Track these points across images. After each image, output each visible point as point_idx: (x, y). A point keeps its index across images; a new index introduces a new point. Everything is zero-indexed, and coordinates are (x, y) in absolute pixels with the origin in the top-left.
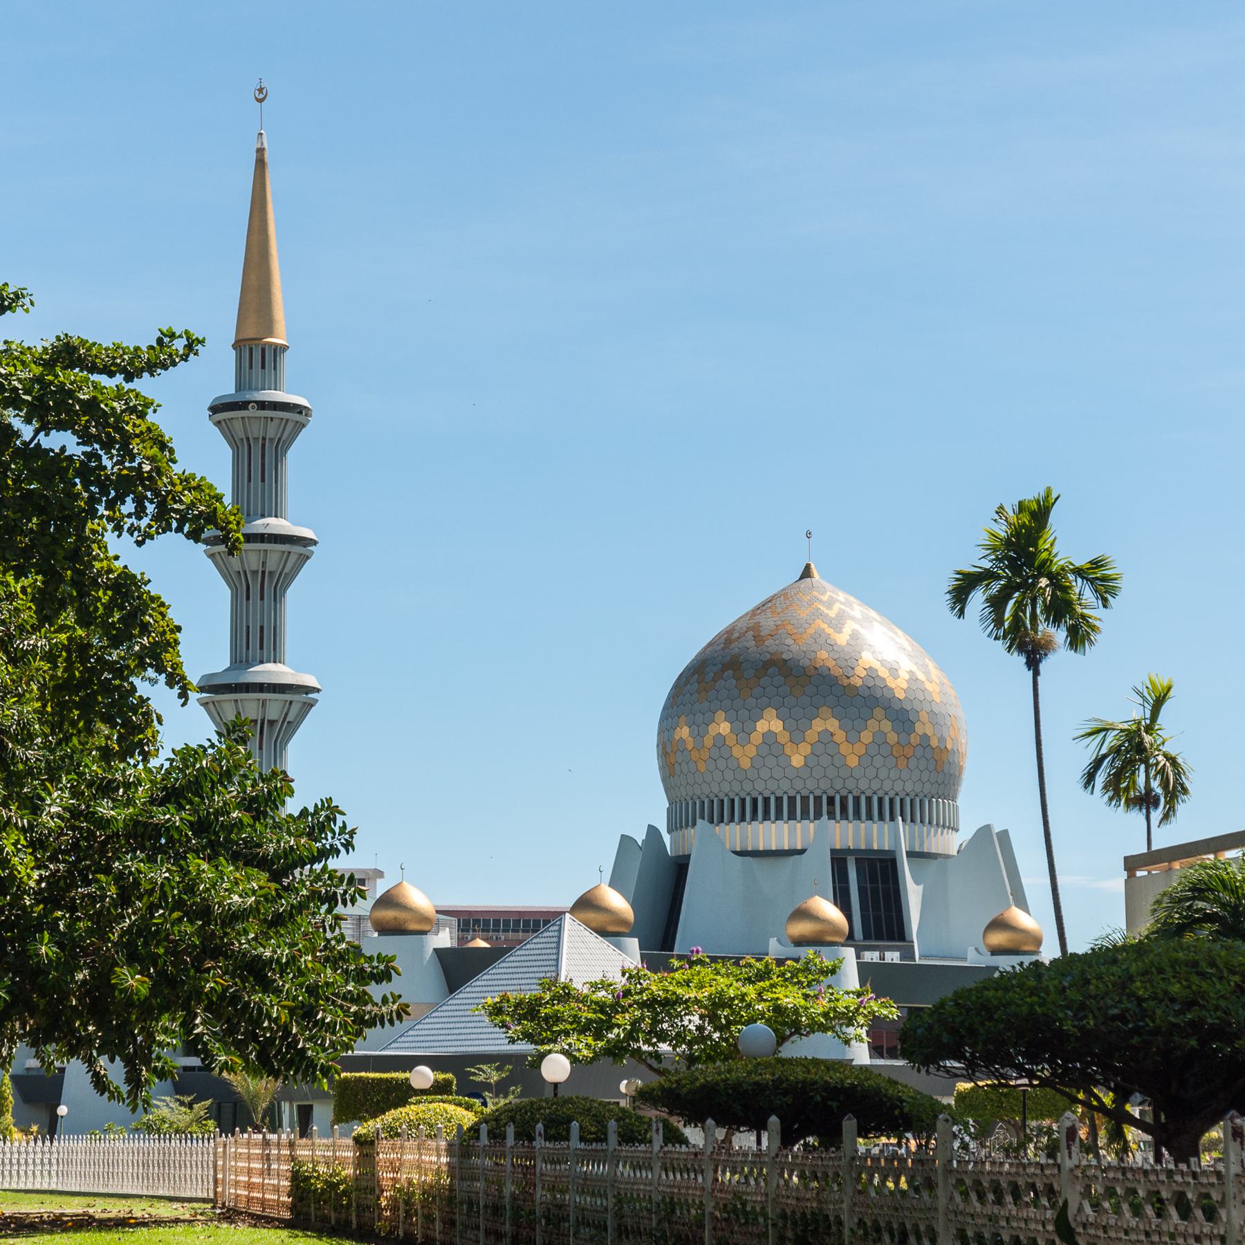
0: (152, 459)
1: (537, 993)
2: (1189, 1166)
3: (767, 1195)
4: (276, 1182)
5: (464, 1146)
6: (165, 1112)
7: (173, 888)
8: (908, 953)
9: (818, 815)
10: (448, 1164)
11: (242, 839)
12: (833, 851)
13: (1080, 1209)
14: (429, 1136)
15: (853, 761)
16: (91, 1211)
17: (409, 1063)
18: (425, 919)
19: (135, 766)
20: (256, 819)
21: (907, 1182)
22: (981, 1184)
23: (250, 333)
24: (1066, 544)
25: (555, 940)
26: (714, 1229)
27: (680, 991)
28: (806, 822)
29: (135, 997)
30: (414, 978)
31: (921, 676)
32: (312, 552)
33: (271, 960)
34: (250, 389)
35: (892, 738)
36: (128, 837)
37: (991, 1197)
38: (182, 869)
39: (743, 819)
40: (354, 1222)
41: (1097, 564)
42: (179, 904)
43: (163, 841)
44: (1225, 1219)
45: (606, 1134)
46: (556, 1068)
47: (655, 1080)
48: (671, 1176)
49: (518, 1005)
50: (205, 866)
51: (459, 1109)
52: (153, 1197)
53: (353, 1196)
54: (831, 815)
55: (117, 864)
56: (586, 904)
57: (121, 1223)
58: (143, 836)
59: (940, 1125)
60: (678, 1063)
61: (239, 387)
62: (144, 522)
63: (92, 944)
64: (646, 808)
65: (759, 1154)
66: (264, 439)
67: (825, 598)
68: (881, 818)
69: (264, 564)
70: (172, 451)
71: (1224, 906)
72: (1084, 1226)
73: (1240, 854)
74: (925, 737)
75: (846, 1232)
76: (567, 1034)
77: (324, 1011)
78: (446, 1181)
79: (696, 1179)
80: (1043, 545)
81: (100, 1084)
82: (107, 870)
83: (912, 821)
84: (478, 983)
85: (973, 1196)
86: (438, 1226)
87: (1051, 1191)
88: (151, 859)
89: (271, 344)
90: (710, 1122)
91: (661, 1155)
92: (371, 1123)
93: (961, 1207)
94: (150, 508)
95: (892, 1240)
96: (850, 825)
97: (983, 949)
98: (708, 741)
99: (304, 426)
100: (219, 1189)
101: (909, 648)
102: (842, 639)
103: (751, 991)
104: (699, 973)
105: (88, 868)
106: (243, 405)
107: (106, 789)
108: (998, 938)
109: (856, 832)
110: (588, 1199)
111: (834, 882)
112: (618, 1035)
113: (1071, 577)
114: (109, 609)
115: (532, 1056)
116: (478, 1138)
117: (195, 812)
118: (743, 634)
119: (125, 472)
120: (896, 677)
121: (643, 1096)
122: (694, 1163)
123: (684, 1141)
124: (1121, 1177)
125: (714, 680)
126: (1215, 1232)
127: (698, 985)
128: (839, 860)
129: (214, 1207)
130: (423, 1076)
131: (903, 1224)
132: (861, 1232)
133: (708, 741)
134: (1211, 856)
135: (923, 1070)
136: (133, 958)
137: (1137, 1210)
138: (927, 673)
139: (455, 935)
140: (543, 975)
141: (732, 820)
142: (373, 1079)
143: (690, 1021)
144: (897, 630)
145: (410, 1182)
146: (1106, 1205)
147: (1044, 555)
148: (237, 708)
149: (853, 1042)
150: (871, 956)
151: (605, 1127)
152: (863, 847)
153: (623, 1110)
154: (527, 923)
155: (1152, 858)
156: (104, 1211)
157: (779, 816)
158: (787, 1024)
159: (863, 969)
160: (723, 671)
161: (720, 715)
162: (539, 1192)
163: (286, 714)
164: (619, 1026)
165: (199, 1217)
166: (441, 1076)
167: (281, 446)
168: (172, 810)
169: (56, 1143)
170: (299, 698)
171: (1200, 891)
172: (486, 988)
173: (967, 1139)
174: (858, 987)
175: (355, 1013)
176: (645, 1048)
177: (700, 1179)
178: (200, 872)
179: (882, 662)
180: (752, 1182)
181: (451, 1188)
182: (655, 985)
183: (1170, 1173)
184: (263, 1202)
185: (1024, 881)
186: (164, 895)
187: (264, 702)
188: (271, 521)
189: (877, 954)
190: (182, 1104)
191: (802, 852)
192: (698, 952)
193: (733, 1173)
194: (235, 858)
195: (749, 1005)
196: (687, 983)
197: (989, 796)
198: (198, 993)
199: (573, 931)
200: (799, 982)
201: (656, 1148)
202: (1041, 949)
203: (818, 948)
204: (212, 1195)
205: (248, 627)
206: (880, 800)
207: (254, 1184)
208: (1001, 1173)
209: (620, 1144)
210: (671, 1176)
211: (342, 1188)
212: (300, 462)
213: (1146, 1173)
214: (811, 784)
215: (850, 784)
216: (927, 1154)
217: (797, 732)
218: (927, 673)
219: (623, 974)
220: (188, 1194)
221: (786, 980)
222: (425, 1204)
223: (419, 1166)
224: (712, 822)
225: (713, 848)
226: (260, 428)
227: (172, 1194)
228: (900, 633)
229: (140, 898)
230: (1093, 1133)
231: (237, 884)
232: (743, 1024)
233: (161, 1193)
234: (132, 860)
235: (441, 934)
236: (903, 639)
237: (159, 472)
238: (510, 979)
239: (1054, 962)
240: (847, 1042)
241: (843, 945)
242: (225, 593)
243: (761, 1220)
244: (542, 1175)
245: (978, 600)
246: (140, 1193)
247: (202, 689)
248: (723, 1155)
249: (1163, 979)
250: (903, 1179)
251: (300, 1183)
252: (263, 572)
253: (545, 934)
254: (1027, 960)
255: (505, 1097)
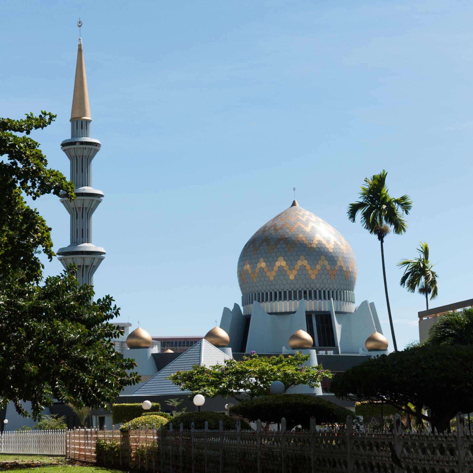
0: (36, 165)
1: (191, 370)
2: (443, 434)
3: (281, 449)
4: (90, 448)
5: (163, 432)
6: (46, 421)
7: (48, 332)
8: (336, 351)
9: (300, 298)
10: (157, 439)
11: (75, 313)
12: (306, 312)
13: (402, 452)
14: (150, 428)
15: (313, 277)
16: (17, 461)
17: (142, 399)
18: (147, 342)
19: (33, 285)
20: (80, 304)
21: (335, 442)
22: (364, 442)
23: (77, 116)
24: (392, 191)
25: (199, 349)
26: (261, 463)
27: (247, 368)
28: (285, 301)
29: (32, 375)
30: (143, 365)
31: (339, 243)
32: (102, 200)
33: (87, 359)
34: (77, 137)
35: (328, 267)
36: (30, 313)
37: (368, 448)
38: (51, 324)
39: (271, 300)
40: (121, 463)
41: (403, 198)
42: (50, 338)
43: (44, 314)
44: (458, 454)
45: (219, 426)
46: (199, 400)
47: (238, 404)
48: (244, 442)
49: (184, 375)
50: (60, 323)
51: (162, 417)
52: (42, 455)
53: (120, 453)
54: (305, 298)
55: (25, 324)
56: (211, 335)
57: (28, 466)
58: (36, 312)
59: (348, 420)
60: (247, 396)
61: (73, 136)
62: (36, 190)
63: (16, 355)
64: (233, 297)
65: (278, 433)
66: (82, 156)
67: (301, 214)
68: (325, 298)
69: (83, 205)
70: (46, 161)
71: (457, 330)
72: (404, 458)
73: (462, 310)
74: (341, 267)
75: (312, 463)
76: (204, 386)
77: (108, 379)
78: (156, 446)
79: (254, 443)
80: (384, 191)
81: (19, 410)
82: (22, 326)
83: (337, 299)
84: (169, 367)
85: (361, 448)
86: (154, 464)
87: (391, 445)
88: (39, 321)
89: (85, 120)
90: (259, 420)
91: (240, 434)
92: (127, 424)
93: (357, 452)
94: (37, 185)
95: (330, 466)
96: (313, 302)
97: (365, 349)
98: (257, 270)
99: (98, 151)
100: (68, 451)
101: (334, 233)
102: (308, 229)
103: (275, 368)
104: (255, 361)
105: (14, 325)
106: (74, 143)
107: (21, 294)
108: (371, 345)
109: (315, 304)
110: (212, 452)
111: (307, 324)
112: (224, 386)
113: (394, 203)
114: (22, 224)
115: (190, 395)
116: (169, 429)
117: (56, 302)
118: (270, 228)
119: (26, 170)
120: (329, 244)
121: (232, 411)
122: (254, 436)
123: (249, 428)
124: (417, 439)
125: (259, 246)
126: (454, 459)
127: (254, 365)
128: (309, 315)
129: (66, 459)
130: (148, 404)
131: (334, 459)
132: (318, 463)
133: (257, 270)
134: (452, 311)
135: (341, 398)
136: (32, 360)
137: (424, 452)
138: (341, 242)
139: (160, 348)
140: (194, 363)
141: (267, 300)
142: (128, 406)
143: (252, 380)
144: (329, 225)
145: (142, 446)
146: (412, 450)
147: (384, 196)
148: (73, 261)
149: (315, 387)
150: (322, 353)
151: (218, 423)
152: (318, 310)
153: (226, 416)
154: (188, 342)
155: (428, 312)
156: (22, 461)
157: (285, 299)
158: (289, 381)
159: (320, 358)
160: (262, 242)
161: (262, 260)
162: (193, 450)
163: (93, 263)
164: (224, 383)
165: (60, 463)
166: (155, 404)
167: (89, 159)
168: (47, 301)
169: (3, 434)
170: (97, 257)
171: (447, 324)
172: (171, 370)
173: (359, 425)
174: (317, 365)
175: (120, 380)
176: (235, 391)
177: (255, 443)
178: (58, 325)
179: (324, 238)
180: (276, 444)
181: (159, 449)
182: (238, 366)
183: (436, 437)
184: (85, 456)
185: (381, 322)
186: (44, 335)
187: (84, 258)
188: (86, 188)
189: (324, 352)
190: (53, 417)
191: (294, 312)
192: (254, 353)
193: (268, 440)
194: (72, 320)
195: (274, 373)
196: (250, 365)
197: (365, 290)
198: (57, 373)
199: (206, 346)
200: (294, 364)
201: (238, 431)
202: (388, 348)
203: (300, 350)
204: (65, 454)
205: (77, 229)
206: (324, 292)
207: (81, 449)
208: (371, 438)
209: (224, 430)
210: (244, 442)
211: (116, 449)
212: (97, 165)
213: (427, 437)
214: (297, 286)
215: (313, 286)
216: (343, 431)
217: (291, 266)
218: (341, 242)
219: (225, 362)
220: (56, 454)
221: (289, 363)
222: (148, 455)
223: (146, 440)
224: (259, 301)
225: (260, 311)
226: (81, 151)
227: (49, 453)
228: (331, 227)
229: (35, 337)
230: (409, 421)
231: (73, 330)
232: (272, 380)
233: (45, 453)
234: (32, 321)
235: (154, 348)
236: (331, 229)
237: (40, 169)
238: (180, 366)
239: (391, 354)
240: (313, 387)
241: (311, 349)
242: (69, 216)
243: (279, 459)
244: (194, 442)
245: (359, 214)
246: (37, 453)
247: (58, 254)
248: (265, 433)
249: (432, 361)
250: (334, 441)
251: (100, 448)
252: (83, 208)
253: (195, 347)
254: (380, 353)
255: (181, 412)
